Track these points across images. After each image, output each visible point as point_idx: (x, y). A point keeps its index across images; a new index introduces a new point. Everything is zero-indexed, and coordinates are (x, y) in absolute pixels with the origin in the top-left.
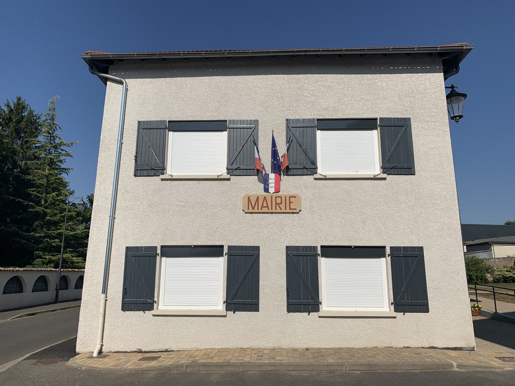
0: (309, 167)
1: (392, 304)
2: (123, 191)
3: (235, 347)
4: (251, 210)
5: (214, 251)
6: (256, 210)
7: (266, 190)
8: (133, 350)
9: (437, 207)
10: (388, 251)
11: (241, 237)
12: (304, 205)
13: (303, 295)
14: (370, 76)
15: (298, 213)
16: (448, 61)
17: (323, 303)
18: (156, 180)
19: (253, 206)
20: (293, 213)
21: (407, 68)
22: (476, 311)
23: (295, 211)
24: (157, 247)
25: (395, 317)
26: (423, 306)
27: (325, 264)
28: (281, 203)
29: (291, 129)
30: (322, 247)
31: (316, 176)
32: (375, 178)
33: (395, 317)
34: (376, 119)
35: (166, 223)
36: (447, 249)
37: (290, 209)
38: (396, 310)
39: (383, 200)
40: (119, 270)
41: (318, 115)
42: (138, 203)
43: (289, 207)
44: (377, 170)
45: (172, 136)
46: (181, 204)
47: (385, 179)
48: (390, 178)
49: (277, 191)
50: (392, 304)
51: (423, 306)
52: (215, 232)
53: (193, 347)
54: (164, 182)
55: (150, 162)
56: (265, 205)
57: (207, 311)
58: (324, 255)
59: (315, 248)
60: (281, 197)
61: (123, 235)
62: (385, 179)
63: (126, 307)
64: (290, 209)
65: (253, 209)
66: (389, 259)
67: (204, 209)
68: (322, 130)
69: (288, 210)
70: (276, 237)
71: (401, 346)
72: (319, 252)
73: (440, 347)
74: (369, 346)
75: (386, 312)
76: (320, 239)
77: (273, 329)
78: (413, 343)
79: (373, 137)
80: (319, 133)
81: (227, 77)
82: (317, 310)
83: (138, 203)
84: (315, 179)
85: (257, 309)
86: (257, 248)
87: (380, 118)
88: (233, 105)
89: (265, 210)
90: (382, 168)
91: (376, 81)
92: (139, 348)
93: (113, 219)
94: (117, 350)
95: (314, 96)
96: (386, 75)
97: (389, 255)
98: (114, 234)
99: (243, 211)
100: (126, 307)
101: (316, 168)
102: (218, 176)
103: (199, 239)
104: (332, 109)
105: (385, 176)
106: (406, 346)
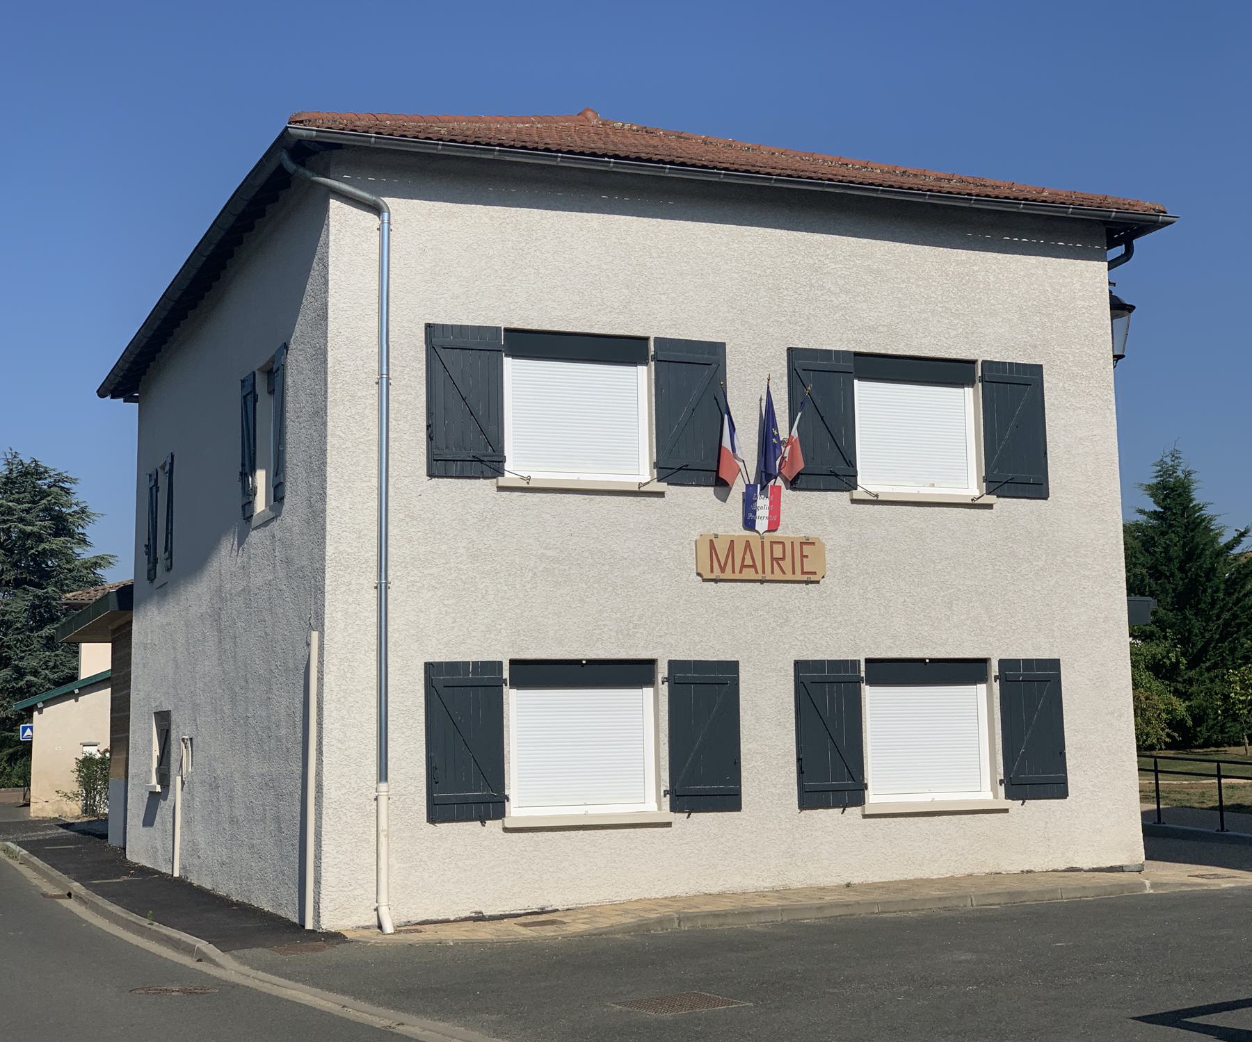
1: (666, 793)
2: (402, 516)
3: (692, 893)
4: (717, 573)
5: (632, 673)
6: (728, 574)
7: (749, 524)
8: (463, 915)
9: (1087, 573)
10: (995, 669)
11: (697, 639)
12: (832, 560)
13: (831, 770)
15: (818, 582)
16: (1110, 232)
17: (511, 797)
18: (484, 487)
19: (722, 565)
20: (807, 582)
21: (1038, 242)
22: (1151, 794)
23: (813, 578)
24: (500, 663)
25: (1006, 811)
26: (1056, 787)
27: (520, 706)
28: (783, 559)
29: (441, 352)
30: (868, 661)
31: (502, 481)
32: (972, 505)
33: (1006, 811)
34: (974, 362)
35: (517, 601)
36: (1102, 665)
37: (803, 573)
38: (674, 809)
39: (985, 554)
40: (411, 722)
41: (855, 340)
42: (444, 547)
43: (796, 565)
44: (642, 472)
45: (864, 391)
46: (549, 553)
47: (990, 506)
48: (672, 491)
49: (773, 526)
50: (1001, 782)
51: (1056, 787)
52: (635, 626)
53: (601, 898)
55: (465, 441)
56: (748, 562)
58: (517, 683)
59: (855, 663)
60: (782, 543)
61: (413, 632)
62: (661, 494)
63: (439, 811)
64: (803, 573)
65: (723, 570)
66: (996, 686)
67: (607, 567)
68: (514, 356)
69: (799, 577)
70: (772, 638)
71: (1016, 869)
72: (506, 675)
73: (1085, 867)
75: (986, 801)
76: (863, 644)
79: (635, 385)
80: (509, 364)
81: (645, 220)
82: (500, 814)
83: (444, 547)
84: (853, 501)
85: (737, 807)
86: (733, 667)
87: (984, 362)
88: (664, 298)
89: (749, 573)
91: (976, 268)
92: (478, 909)
93: (382, 588)
94: (424, 918)
95: (847, 292)
96: (995, 255)
97: (996, 678)
98: (390, 629)
99: (699, 574)
100: (439, 811)
101: (502, 460)
102: (640, 485)
103: (599, 645)
104: (885, 329)
105: (662, 486)
106: (1027, 868)
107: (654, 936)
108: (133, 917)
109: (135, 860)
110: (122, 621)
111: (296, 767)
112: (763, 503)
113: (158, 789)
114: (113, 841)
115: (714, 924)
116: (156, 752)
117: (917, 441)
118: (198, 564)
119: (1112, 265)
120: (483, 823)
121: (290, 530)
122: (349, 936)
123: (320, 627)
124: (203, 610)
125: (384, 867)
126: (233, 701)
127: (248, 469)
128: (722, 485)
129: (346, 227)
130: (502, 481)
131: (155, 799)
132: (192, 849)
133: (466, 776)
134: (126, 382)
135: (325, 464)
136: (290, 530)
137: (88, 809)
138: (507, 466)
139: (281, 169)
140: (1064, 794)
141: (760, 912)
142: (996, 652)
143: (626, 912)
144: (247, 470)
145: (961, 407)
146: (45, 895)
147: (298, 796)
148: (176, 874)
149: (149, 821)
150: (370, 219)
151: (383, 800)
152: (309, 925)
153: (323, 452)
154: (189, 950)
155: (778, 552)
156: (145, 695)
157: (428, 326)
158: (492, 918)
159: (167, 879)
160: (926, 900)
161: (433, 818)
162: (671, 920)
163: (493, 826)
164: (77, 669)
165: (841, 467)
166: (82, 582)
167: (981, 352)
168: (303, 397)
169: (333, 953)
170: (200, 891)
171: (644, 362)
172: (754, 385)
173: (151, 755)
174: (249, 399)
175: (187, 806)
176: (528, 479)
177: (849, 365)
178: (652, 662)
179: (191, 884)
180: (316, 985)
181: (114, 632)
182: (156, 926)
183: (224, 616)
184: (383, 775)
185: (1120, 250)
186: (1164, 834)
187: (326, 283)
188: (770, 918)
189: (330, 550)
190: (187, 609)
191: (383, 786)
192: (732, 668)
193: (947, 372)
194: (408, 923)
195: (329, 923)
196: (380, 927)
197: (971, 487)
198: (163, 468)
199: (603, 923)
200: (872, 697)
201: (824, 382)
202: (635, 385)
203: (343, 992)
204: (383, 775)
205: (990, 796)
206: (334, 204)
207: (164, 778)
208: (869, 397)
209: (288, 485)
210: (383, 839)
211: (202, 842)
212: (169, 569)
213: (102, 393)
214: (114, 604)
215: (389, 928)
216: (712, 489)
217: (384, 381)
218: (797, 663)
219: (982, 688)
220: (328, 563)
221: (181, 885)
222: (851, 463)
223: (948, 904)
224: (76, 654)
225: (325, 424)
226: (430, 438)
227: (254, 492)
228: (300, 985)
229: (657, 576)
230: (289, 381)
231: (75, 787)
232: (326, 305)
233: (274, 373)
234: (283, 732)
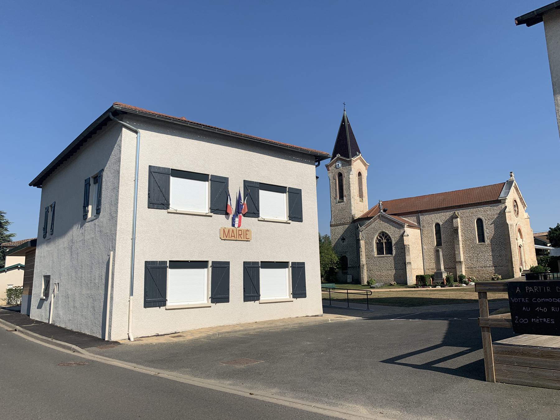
0: (254, 212)
4: (225, 238)
5: (202, 264)
13: (252, 292)
14: (284, 160)
18: (164, 212)
19: (226, 236)
31: (169, 210)
34: (286, 187)
38: (212, 302)
43: (244, 237)
45: (262, 193)
47: (290, 223)
49: (239, 226)
54: (170, 214)
55: (159, 199)
57: (202, 304)
58: (171, 267)
59: (258, 262)
63: (147, 304)
66: (291, 269)
68: (173, 176)
72: (168, 265)
74: (286, 317)
77: (237, 314)
78: (300, 315)
79: (206, 186)
82: (165, 305)
84: (259, 220)
85: (228, 301)
90: (210, 208)
93: (133, 239)
100: (147, 304)
105: (212, 214)
107: (213, 339)
108: (44, 338)
109: (33, 318)
110: (32, 249)
111: (102, 292)
112: (237, 220)
113: (44, 298)
114: (24, 312)
115: (227, 335)
116: (43, 287)
117: (273, 205)
118: (63, 233)
119: (316, 166)
120: (160, 307)
121: (102, 222)
122: (121, 342)
123: (114, 249)
124: (65, 246)
125: (131, 322)
126: (76, 272)
127: (86, 205)
128: (227, 214)
129: (127, 137)
130: (169, 210)
131: (42, 301)
132: (57, 315)
133: (155, 294)
134: (38, 182)
135: (118, 203)
136: (102, 222)
137: (8, 303)
138: (170, 206)
139: (109, 117)
140: (305, 297)
141: (239, 331)
142: (291, 260)
143: (201, 332)
144: (86, 205)
145: (283, 198)
146: (7, 330)
147: (102, 300)
148: (50, 323)
149: (40, 307)
150: (134, 135)
151: (131, 301)
152: (106, 339)
153: (117, 200)
154: (69, 348)
155: (240, 233)
156: (40, 269)
157: (150, 166)
158: (161, 335)
159: (47, 324)
160: (280, 326)
161: (145, 307)
162: (216, 334)
163: (163, 308)
164: (4, 263)
165: (256, 212)
166: (5, 240)
167: (288, 185)
168: (109, 184)
169: (117, 348)
170: (61, 328)
171: (208, 181)
172: (235, 190)
173: (41, 288)
174: (87, 184)
175: (56, 303)
176: (176, 210)
177: (258, 186)
178: (207, 262)
179: (57, 326)
180: (120, 360)
181: (27, 253)
182: (54, 341)
183: (73, 247)
184: (132, 294)
185: (317, 163)
186: (329, 305)
187: (120, 151)
188: (240, 333)
189: (118, 228)
190: (58, 246)
191: (131, 297)
192: (228, 263)
193: (279, 189)
194: (137, 338)
195: (113, 339)
196: (129, 339)
197: (285, 218)
198: (51, 206)
199: (197, 336)
200: (262, 271)
201: (252, 189)
202: (206, 186)
203: (134, 362)
204: (132, 294)
205: (288, 297)
206: (124, 129)
207: (46, 294)
208: (263, 194)
209: (102, 209)
210: (131, 313)
211: (61, 313)
212: (52, 234)
213: (30, 185)
214: (29, 245)
215: (132, 339)
216: (224, 216)
217: (136, 181)
218: (244, 262)
219: (287, 269)
220: (118, 232)
221: (52, 326)
222: (258, 211)
223: (285, 327)
224: (4, 259)
225: (118, 191)
226: (149, 197)
227: (88, 211)
228: (114, 360)
229: (208, 238)
230: (104, 180)
231: (6, 297)
232: (120, 158)
233: (98, 179)
234: (97, 281)
